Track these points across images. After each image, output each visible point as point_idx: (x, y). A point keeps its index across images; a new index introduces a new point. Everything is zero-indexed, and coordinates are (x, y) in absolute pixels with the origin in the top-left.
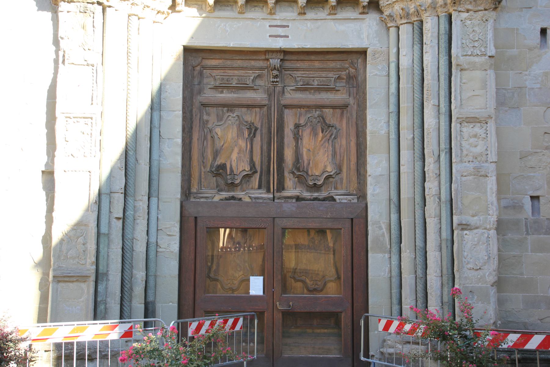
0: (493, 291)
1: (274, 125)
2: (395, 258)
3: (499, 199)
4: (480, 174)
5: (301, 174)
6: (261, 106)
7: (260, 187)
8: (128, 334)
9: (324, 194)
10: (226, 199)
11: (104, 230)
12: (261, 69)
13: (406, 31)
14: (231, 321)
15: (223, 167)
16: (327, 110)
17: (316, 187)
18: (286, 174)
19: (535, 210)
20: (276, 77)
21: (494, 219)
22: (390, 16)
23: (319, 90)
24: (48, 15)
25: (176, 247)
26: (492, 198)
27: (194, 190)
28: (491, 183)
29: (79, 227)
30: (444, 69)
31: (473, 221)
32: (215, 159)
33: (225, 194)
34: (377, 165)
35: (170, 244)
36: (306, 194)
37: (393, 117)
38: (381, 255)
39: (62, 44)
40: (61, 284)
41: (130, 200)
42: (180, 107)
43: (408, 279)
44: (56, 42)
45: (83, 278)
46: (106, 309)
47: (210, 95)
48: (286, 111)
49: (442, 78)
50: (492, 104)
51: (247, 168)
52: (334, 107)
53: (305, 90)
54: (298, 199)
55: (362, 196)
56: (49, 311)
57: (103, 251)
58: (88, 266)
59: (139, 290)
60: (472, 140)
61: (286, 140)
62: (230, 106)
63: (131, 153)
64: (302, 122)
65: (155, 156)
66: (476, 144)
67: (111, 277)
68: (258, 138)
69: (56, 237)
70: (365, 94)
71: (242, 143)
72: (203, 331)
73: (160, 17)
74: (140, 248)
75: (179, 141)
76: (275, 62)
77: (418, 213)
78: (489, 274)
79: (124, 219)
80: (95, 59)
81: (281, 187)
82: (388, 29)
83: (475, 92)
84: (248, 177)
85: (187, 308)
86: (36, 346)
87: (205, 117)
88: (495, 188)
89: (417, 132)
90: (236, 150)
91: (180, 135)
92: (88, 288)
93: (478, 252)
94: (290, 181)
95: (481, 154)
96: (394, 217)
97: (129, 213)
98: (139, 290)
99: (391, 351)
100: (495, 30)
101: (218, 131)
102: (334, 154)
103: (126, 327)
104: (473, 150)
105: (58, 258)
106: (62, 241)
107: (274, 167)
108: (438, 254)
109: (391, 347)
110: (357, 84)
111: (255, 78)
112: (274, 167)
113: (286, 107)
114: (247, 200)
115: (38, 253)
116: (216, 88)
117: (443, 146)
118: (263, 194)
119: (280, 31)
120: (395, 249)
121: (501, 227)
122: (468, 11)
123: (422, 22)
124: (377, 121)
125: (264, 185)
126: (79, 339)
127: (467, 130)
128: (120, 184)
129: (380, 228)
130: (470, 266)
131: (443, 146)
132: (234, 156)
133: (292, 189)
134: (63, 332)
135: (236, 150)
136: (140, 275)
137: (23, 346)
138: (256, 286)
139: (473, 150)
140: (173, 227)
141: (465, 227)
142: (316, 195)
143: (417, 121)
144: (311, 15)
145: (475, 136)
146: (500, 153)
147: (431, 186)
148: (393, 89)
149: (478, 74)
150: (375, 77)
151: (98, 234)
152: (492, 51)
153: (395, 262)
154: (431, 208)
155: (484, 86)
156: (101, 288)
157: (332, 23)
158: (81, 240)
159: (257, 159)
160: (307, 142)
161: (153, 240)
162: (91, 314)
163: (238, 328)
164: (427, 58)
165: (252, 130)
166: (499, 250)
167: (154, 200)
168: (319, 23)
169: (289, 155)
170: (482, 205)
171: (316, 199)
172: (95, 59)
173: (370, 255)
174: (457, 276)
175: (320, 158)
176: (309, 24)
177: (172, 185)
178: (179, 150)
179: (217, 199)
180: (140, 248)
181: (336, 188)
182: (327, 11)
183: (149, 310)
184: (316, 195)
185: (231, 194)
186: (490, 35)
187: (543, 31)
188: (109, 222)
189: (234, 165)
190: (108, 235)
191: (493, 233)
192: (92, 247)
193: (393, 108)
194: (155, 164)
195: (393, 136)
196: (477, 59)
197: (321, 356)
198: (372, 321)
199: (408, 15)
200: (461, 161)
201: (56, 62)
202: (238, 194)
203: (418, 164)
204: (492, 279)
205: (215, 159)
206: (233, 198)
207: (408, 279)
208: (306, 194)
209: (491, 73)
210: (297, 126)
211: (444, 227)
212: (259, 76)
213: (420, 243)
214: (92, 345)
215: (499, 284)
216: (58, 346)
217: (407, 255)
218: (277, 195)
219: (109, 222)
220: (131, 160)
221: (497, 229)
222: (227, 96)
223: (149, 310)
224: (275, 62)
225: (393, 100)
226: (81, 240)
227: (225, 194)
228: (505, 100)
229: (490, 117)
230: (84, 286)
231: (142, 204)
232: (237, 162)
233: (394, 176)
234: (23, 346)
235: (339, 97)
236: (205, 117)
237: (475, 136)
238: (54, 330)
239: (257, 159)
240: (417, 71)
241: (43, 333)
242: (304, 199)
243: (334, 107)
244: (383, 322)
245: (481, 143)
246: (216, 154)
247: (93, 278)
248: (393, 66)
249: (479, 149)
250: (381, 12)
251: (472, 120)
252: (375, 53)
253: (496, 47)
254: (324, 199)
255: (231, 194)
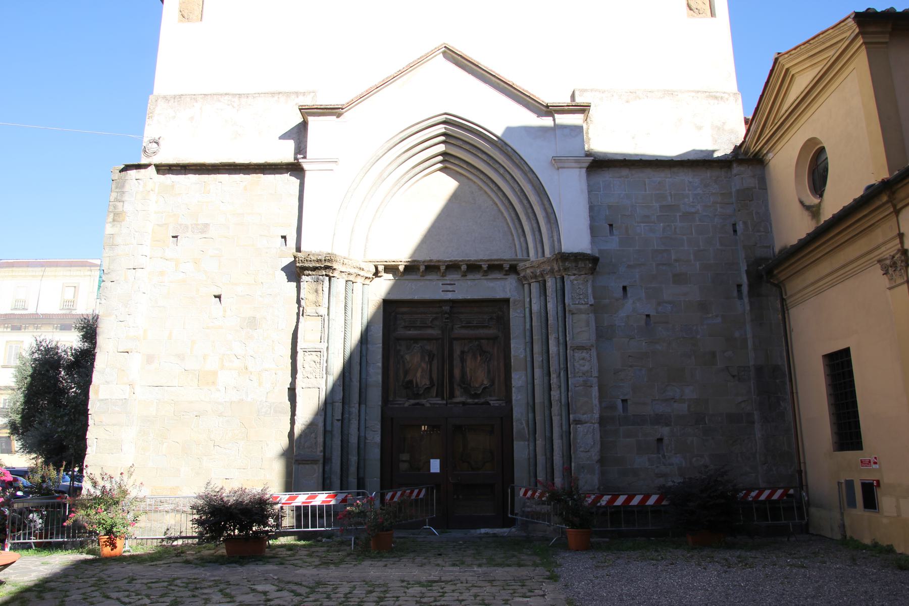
0: (597, 467)
1: (446, 352)
2: (532, 445)
3: (600, 402)
4: (587, 385)
5: (467, 388)
6: (437, 339)
7: (437, 396)
8: (344, 500)
9: (482, 400)
10: (414, 405)
11: (329, 428)
12: (437, 313)
13: (535, 287)
14: (416, 491)
15: (411, 382)
16: (483, 341)
17: (476, 396)
18: (455, 386)
19: (625, 409)
20: (447, 318)
21: (597, 416)
22: (524, 277)
23: (477, 327)
24: (295, 284)
25: (378, 439)
26: (596, 401)
27: (391, 399)
28: (595, 391)
29: (311, 427)
30: (560, 314)
31: (584, 417)
32: (405, 377)
33: (412, 401)
34: (518, 379)
35: (375, 437)
36: (470, 401)
37: (529, 345)
38: (522, 443)
39: (303, 302)
40: (301, 466)
41: (346, 407)
42: (381, 341)
43: (541, 459)
44: (299, 301)
45: (314, 462)
46: (331, 482)
47: (401, 332)
48: (455, 342)
49: (560, 319)
50: (593, 337)
51: (428, 383)
52: (488, 339)
53: (468, 327)
54: (464, 404)
55: (509, 401)
56: (292, 484)
57: (328, 443)
58: (319, 452)
59: (353, 469)
60: (581, 362)
61: (455, 362)
62: (415, 340)
63: (347, 374)
64: (466, 349)
65: (364, 376)
66: (585, 364)
67: (334, 461)
68: (435, 361)
69: (298, 430)
70: (509, 329)
71: (423, 365)
72: (395, 499)
73: (367, 281)
74: (354, 440)
75: (380, 365)
76: (446, 308)
77: (547, 412)
78: (595, 454)
79: (342, 420)
80: (323, 311)
81: (452, 395)
82: (523, 285)
83: (582, 329)
84: (428, 390)
85: (388, 481)
86: (286, 507)
87: (398, 348)
88: (597, 394)
89: (545, 356)
90: (420, 370)
91: (381, 361)
92: (318, 469)
93: (587, 438)
94: (458, 392)
95: (587, 372)
96: (531, 415)
97: (346, 416)
98: (353, 469)
99: (529, 509)
100: (594, 287)
101: (408, 357)
102: (489, 371)
103: (343, 495)
104: (582, 368)
105: (298, 448)
106: (300, 436)
107: (446, 380)
108: (560, 441)
109: (528, 507)
110: (503, 323)
111: (433, 320)
112: (446, 380)
113: (456, 339)
114: (428, 405)
115: (284, 442)
116: (406, 327)
117: (562, 366)
118: (439, 401)
119: (449, 288)
120: (531, 439)
121: (602, 421)
122: (574, 275)
123: (545, 281)
124: (517, 348)
125: (440, 394)
126: (312, 504)
127: (578, 355)
128: (339, 396)
129: (522, 424)
130: (582, 449)
131: (562, 366)
132: (419, 374)
133: (459, 398)
134: (301, 499)
135: (420, 370)
136: (354, 459)
137: (278, 507)
138: (435, 466)
139: (582, 368)
140: (376, 425)
141: (578, 422)
142: (476, 401)
143: (545, 348)
144: (470, 276)
145: (583, 359)
146: (600, 371)
147: (555, 394)
148: (528, 326)
149: (583, 316)
150: (515, 317)
151: (325, 431)
152: (591, 301)
153: (531, 448)
154: (555, 409)
155: (588, 325)
156: (327, 468)
157: (485, 282)
158: (313, 435)
159: (435, 376)
160: (470, 364)
161: (362, 434)
162: (321, 487)
163: (421, 496)
164: (550, 306)
165: (431, 357)
166: (601, 437)
167: (363, 406)
168: (476, 282)
169: (457, 372)
170: (590, 407)
171: (476, 404)
172: (323, 311)
173: (515, 443)
174: (573, 456)
175: (480, 377)
176: (469, 282)
177: (375, 395)
178: (380, 371)
179: (406, 405)
180: (354, 440)
181: (491, 396)
182: (481, 274)
183: (361, 484)
184: (476, 401)
185: (417, 401)
186: (590, 291)
187: (624, 288)
188: (332, 423)
189: (418, 380)
190: (331, 432)
191: (596, 426)
192: (320, 440)
193: (528, 339)
194: (363, 381)
195: (529, 359)
196: (582, 307)
197: (483, 531)
198: (516, 489)
199: (535, 277)
200: (575, 377)
201: (298, 314)
202: (423, 401)
203: (546, 379)
204: (596, 458)
205: (405, 377)
206: (418, 404)
207: (541, 459)
208: (470, 401)
209: (592, 316)
210: (463, 352)
211: (564, 422)
212: (436, 318)
213: (548, 434)
214: (321, 507)
215: (602, 461)
216: (298, 508)
217: (540, 442)
218: (449, 401)
219: (332, 423)
220: (347, 379)
221: (600, 423)
222: (412, 332)
223: (361, 484)
224: (446, 308)
225: (528, 334)
226: (313, 435)
227: (412, 401)
228: (603, 334)
229: (592, 346)
230: (315, 467)
231: (355, 410)
232: (421, 378)
233: (530, 386)
234: (278, 507)
235: (492, 332)
236: (398, 348)
237: (583, 359)
238: (296, 497)
239: (435, 376)
240: (543, 314)
241: (288, 499)
242: (469, 404)
243: (488, 339)
244: (523, 490)
245: (587, 363)
246: (406, 373)
247: (321, 461)
248: (527, 310)
249: (586, 368)
250: (518, 274)
251: (581, 348)
252: (515, 301)
253: (594, 298)
254: (482, 404)
255: (417, 401)
